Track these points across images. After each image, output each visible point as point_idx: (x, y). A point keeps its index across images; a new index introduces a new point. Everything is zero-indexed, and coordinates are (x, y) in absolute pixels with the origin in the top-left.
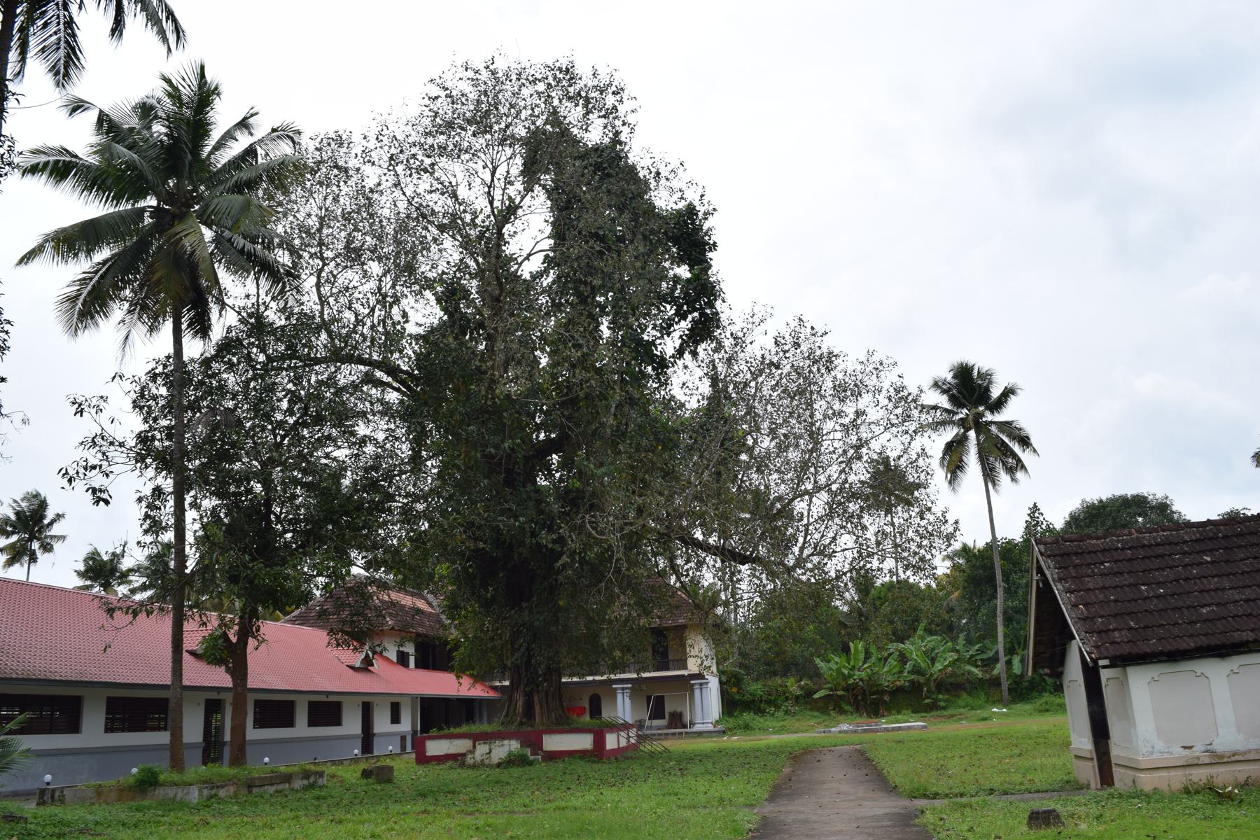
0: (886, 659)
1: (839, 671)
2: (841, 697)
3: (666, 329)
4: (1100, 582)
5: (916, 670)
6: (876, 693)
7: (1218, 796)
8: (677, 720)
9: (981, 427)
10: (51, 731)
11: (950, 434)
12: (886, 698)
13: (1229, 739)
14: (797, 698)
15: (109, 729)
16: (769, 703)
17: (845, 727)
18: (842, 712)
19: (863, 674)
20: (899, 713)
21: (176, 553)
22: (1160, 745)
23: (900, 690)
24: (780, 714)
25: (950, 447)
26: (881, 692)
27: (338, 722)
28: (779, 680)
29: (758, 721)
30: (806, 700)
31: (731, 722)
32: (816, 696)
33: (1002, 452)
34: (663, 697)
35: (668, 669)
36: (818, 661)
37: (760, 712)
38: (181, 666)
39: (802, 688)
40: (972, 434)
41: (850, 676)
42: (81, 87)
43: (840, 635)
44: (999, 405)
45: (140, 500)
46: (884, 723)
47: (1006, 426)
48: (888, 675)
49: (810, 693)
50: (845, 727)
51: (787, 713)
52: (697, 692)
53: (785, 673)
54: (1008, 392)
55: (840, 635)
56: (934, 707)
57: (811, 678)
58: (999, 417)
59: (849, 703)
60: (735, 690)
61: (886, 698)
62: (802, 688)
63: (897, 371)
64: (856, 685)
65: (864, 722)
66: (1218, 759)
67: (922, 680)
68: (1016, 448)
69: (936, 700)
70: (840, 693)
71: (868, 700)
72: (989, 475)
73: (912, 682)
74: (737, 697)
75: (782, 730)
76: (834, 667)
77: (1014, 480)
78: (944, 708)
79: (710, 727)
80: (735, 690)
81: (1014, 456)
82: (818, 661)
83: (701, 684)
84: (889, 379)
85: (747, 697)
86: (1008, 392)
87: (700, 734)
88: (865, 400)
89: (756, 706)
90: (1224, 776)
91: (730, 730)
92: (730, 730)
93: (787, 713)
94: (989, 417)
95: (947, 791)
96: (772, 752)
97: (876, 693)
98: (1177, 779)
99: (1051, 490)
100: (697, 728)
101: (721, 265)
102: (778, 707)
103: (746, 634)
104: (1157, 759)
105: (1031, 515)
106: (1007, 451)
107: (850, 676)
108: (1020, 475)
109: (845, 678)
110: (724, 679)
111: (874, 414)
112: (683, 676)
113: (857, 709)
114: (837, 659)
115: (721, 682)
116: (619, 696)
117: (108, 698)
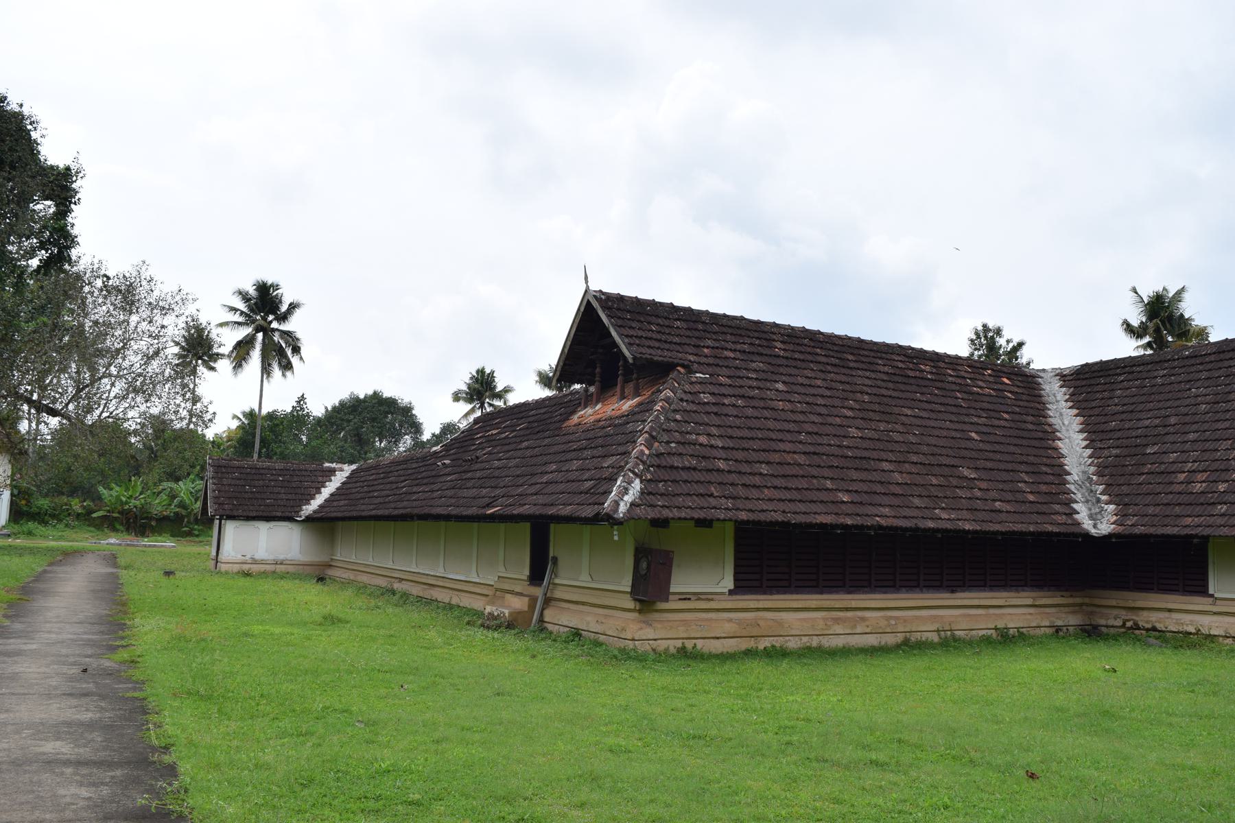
0: (160, 493)
1: (118, 497)
2: (116, 518)
3: (31, 254)
4: (230, 481)
5: (182, 505)
6: (146, 518)
7: (247, 574)
9: (266, 330)
11: (245, 331)
12: (153, 523)
13: (261, 554)
14: (78, 515)
16: (53, 516)
17: (112, 541)
18: (114, 530)
19: (138, 503)
20: (160, 535)
22: (233, 554)
23: (166, 518)
24: (61, 526)
25: (239, 345)
26: (151, 519)
28: (65, 499)
29: (41, 529)
30: (85, 518)
31: (16, 528)
32: (94, 515)
33: (280, 353)
36: (101, 489)
37: (44, 523)
39: (84, 507)
40: (260, 336)
41: (127, 503)
43: (133, 465)
44: (283, 318)
46: (145, 541)
47: (287, 335)
48: (158, 506)
49: (90, 512)
50: (112, 541)
51: (67, 525)
53: (72, 494)
54: (293, 306)
55: (133, 465)
56: (190, 534)
57: (93, 500)
58: (285, 327)
59: (122, 524)
60: (23, 502)
61: (153, 523)
62: (84, 507)
63: (197, 305)
64: (130, 511)
65: (129, 538)
66: (255, 562)
67: (184, 512)
68: (289, 352)
69: (193, 529)
70: (116, 515)
71: (138, 523)
72: (266, 370)
73: (176, 514)
75: (61, 538)
76: (114, 494)
77: (284, 375)
78: (197, 536)
80: (23, 502)
81: (286, 356)
82: (101, 489)
84: (190, 309)
85: (34, 509)
86: (293, 306)
88: (169, 320)
89: (40, 517)
90: (255, 568)
91: (15, 534)
92: (15, 534)
93: (67, 525)
94: (275, 325)
96: (51, 550)
97: (146, 518)
98: (236, 568)
99: (318, 383)
101: (81, 220)
102: (60, 520)
103: (42, 457)
104: (230, 559)
105: (299, 402)
106: (281, 353)
107: (127, 503)
108: (288, 374)
109: (122, 504)
110: (16, 492)
111: (170, 331)
113: (127, 530)
114: (117, 489)
115: (12, 495)
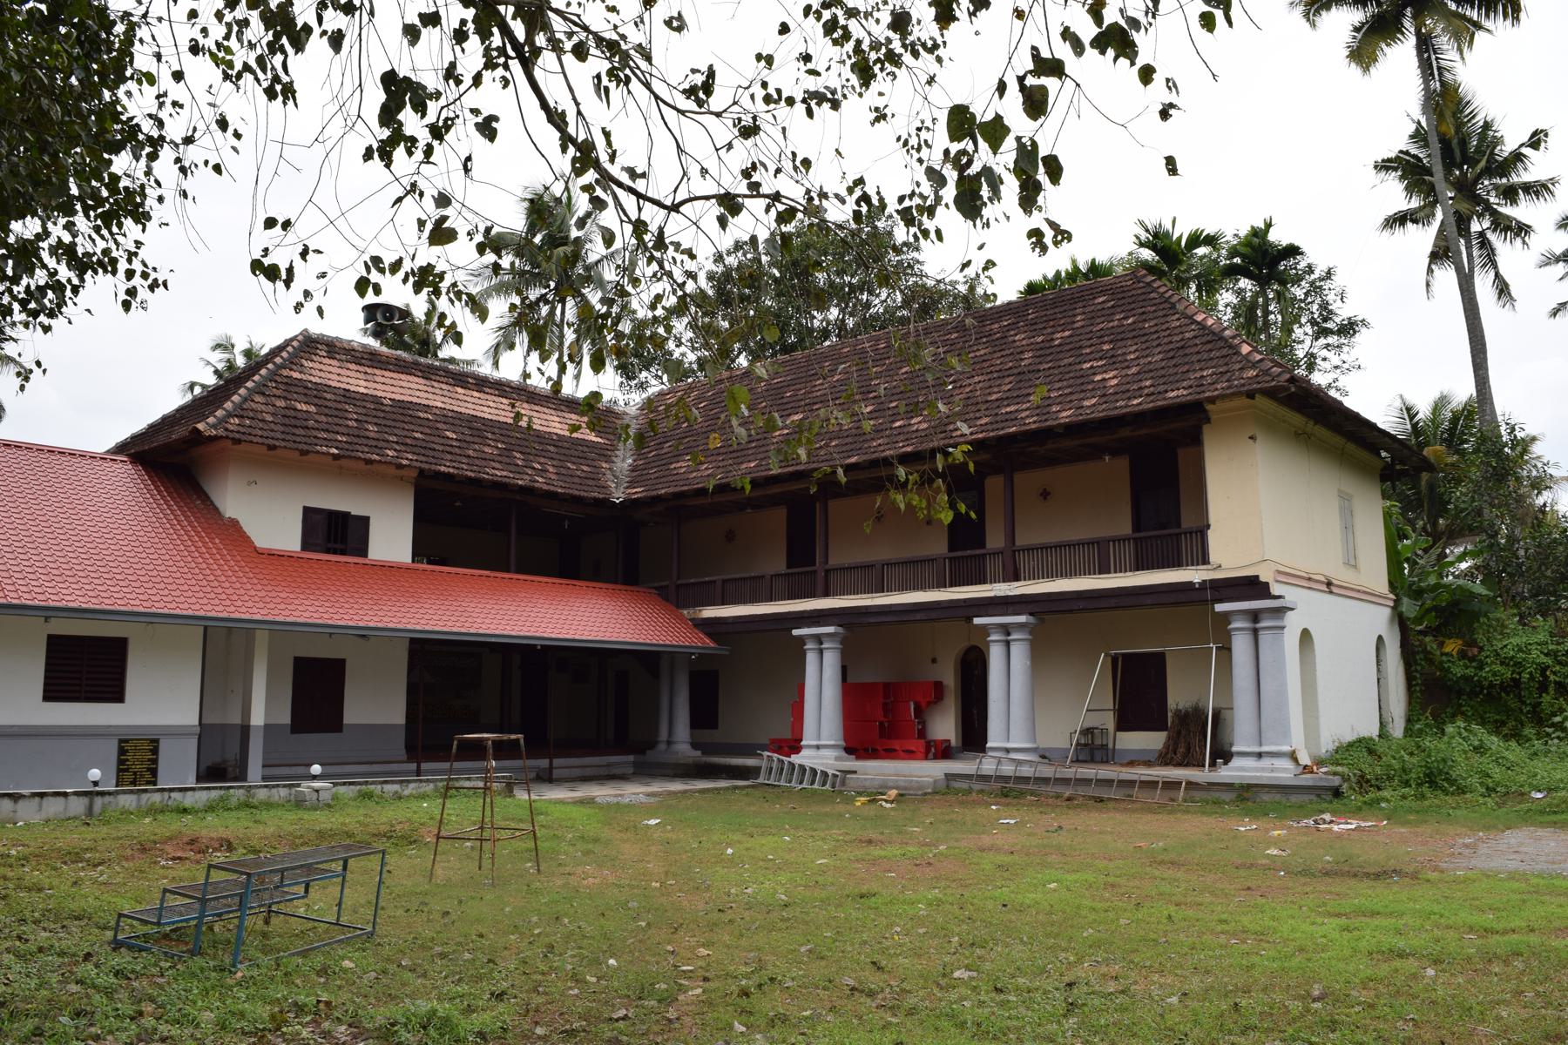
8: (1198, 737)
10: (1287, 719)
15: (51, 694)
21: (228, 398)
27: (115, 693)
34: (1159, 660)
35: (982, 580)
38: (1476, 375)
42: (324, 27)
45: (919, 22)
52: (1241, 645)
74: (1458, 670)
79: (1283, 772)
83: (1255, 616)
85: (1493, 671)
87: (1246, 795)
95: (160, 817)
100: (1238, 770)
112: (1188, 586)
116: (811, 658)
117: (50, 637)
